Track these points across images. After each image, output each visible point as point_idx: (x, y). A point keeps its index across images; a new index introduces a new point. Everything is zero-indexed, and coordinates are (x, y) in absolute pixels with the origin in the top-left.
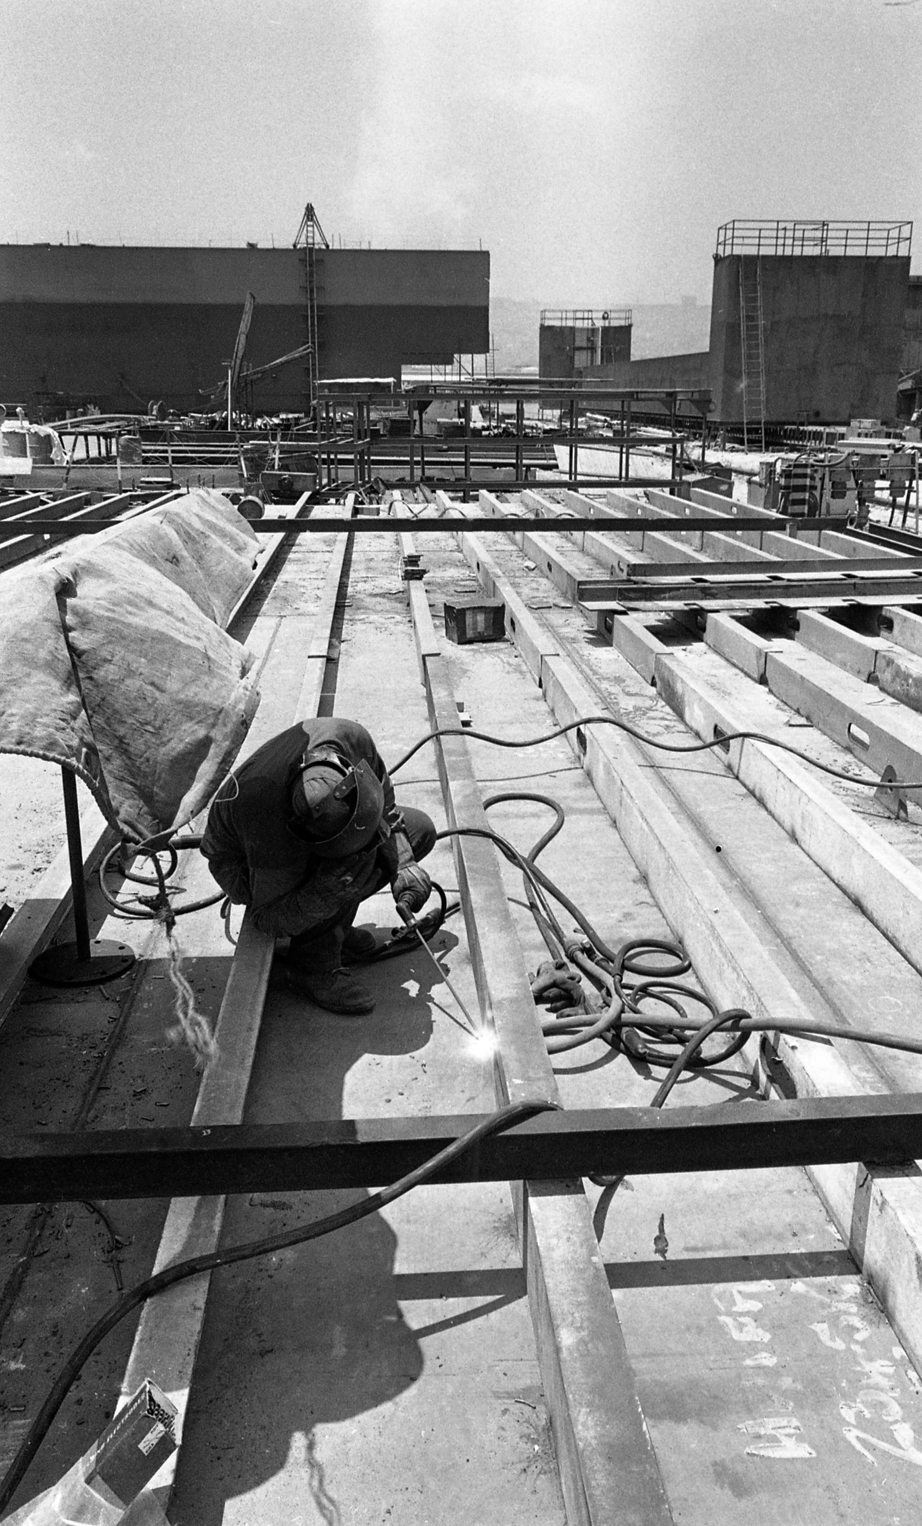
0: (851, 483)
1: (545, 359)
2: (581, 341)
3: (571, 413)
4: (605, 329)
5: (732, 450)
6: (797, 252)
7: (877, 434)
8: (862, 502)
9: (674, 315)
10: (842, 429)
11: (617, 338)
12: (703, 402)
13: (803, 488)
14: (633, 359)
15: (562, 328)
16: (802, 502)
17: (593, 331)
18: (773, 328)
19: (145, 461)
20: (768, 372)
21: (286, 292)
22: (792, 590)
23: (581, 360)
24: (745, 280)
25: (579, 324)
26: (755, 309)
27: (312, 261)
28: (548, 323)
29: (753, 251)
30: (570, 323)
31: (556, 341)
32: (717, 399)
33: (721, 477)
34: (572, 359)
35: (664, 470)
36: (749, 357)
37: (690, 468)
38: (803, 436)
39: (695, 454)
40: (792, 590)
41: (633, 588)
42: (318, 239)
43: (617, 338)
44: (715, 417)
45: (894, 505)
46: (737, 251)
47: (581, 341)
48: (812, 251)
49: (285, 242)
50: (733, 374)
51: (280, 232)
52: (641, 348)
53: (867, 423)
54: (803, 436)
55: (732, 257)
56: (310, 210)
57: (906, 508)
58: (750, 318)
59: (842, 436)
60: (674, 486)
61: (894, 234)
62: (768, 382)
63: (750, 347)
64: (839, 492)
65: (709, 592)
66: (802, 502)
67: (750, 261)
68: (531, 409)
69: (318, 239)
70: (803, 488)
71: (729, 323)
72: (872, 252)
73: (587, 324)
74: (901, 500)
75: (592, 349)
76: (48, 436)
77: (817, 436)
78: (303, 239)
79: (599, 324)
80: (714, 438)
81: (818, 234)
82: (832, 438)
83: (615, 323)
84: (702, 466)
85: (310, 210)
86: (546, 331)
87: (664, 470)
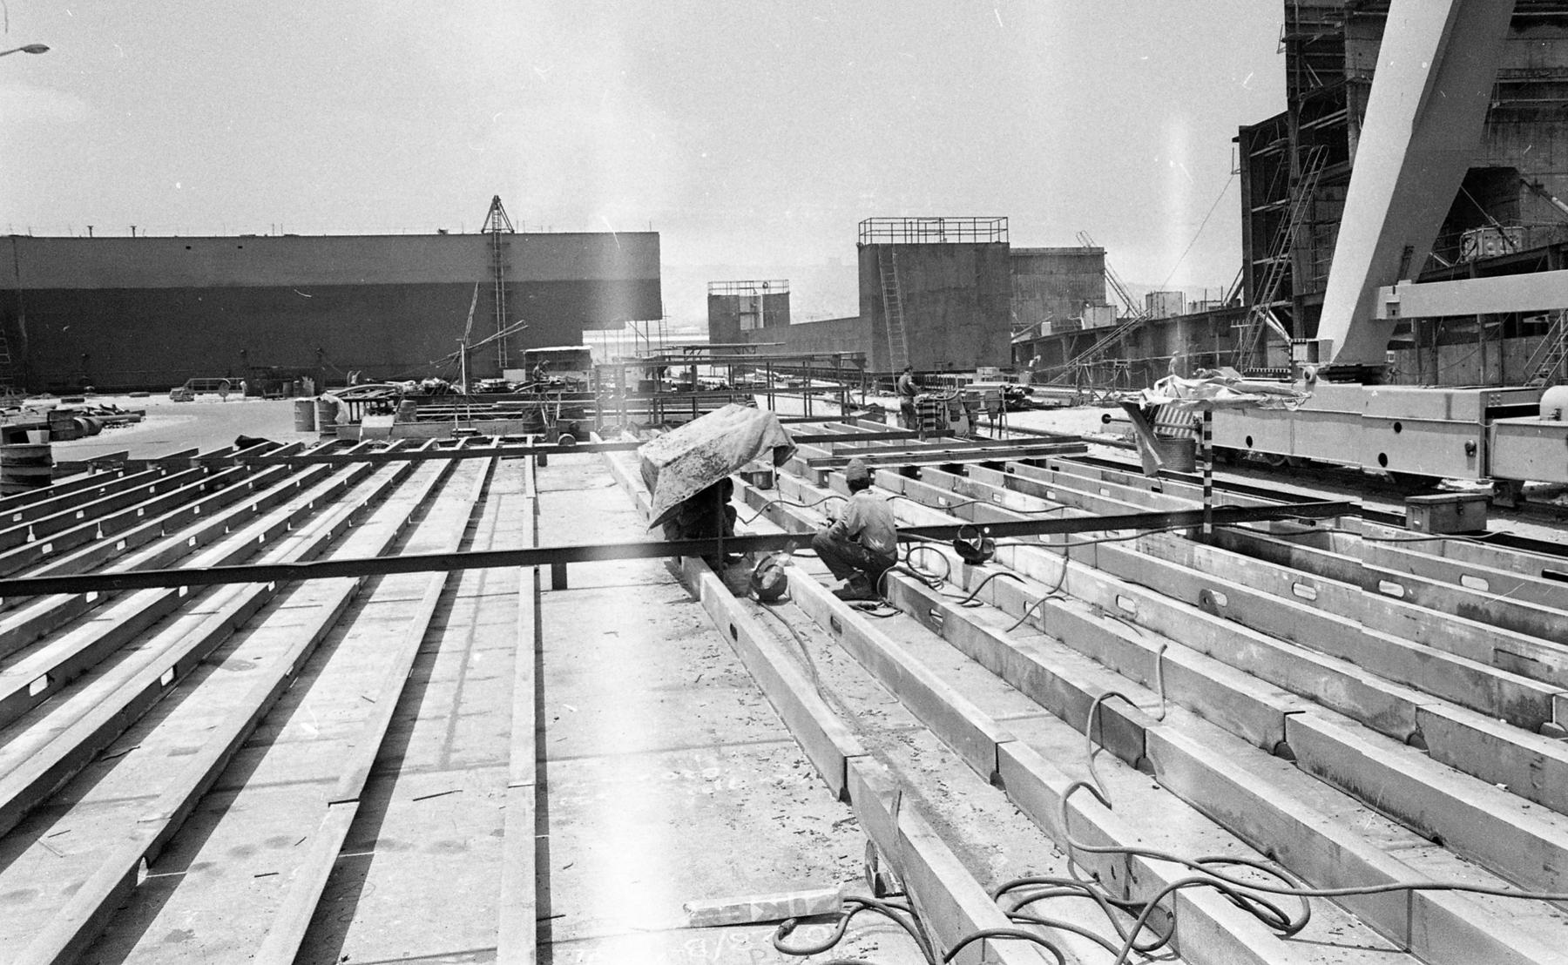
0: (963, 411)
1: (714, 325)
2: (745, 307)
3: (739, 368)
4: (766, 297)
5: (885, 395)
6: (922, 241)
7: (997, 378)
8: (971, 423)
9: (825, 291)
10: (969, 376)
11: (777, 305)
12: (861, 361)
13: (931, 416)
14: (793, 321)
15: (727, 298)
16: (931, 425)
17: (756, 298)
18: (909, 298)
19: (419, 419)
20: (908, 334)
21: (475, 271)
22: (916, 458)
23: (746, 324)
24: (881, 264)
25: (743, 293)
26: (893, 284)
27: (498, 244)
28: (715, 293)
29: (887, 240)
30: (735, 293)
31: (722, 310)
32: (869, 357)
33: (877, 412)
34: (738, 322)
35: (836, 411)
36: (892, 321)
37: (854, 408)
38: (940, 382)
39: (857, 399)
40: (916, 458)
41: (838, 461)
42: (504, 225)
43: (777, 305)
44: (869, 370)
45: (992, 426)
46: (876, 241)
47: (745, 307)
48: (933, 239)
49: (474, 229)
50: (879, 335)
51: (472, 222)
52: (799, 313)
53: (989, 370)
54: (940, 382)
55: (872, 245)
56: (496, 200)
57: (1000, 427)
58: (890, 292)
59: (971, 381)
60: (843, 419)
61: (995, 226)
62: (909, 341)
63: (893, 314)
64: (955, 418)
65: (874, 461)
66: (931, 425)
67: (887, 248)
68: (703, 370)
69: (504, 225)
70: (931, 416)
71: (872, 299)
72: (980, 239)
73: (749, 293)
74: (996, 422)
75: (756, 314)
76: (336, 404)
77: (951, 382)
78: (490, 226)
79: (760, 292)
80: (870, 386)
81: (937, 227)
82: (962, 382)
83: (773, 292)
84: (864, 407)
85: (496, 200)
86: (713, 300)
87: (836, 411)
